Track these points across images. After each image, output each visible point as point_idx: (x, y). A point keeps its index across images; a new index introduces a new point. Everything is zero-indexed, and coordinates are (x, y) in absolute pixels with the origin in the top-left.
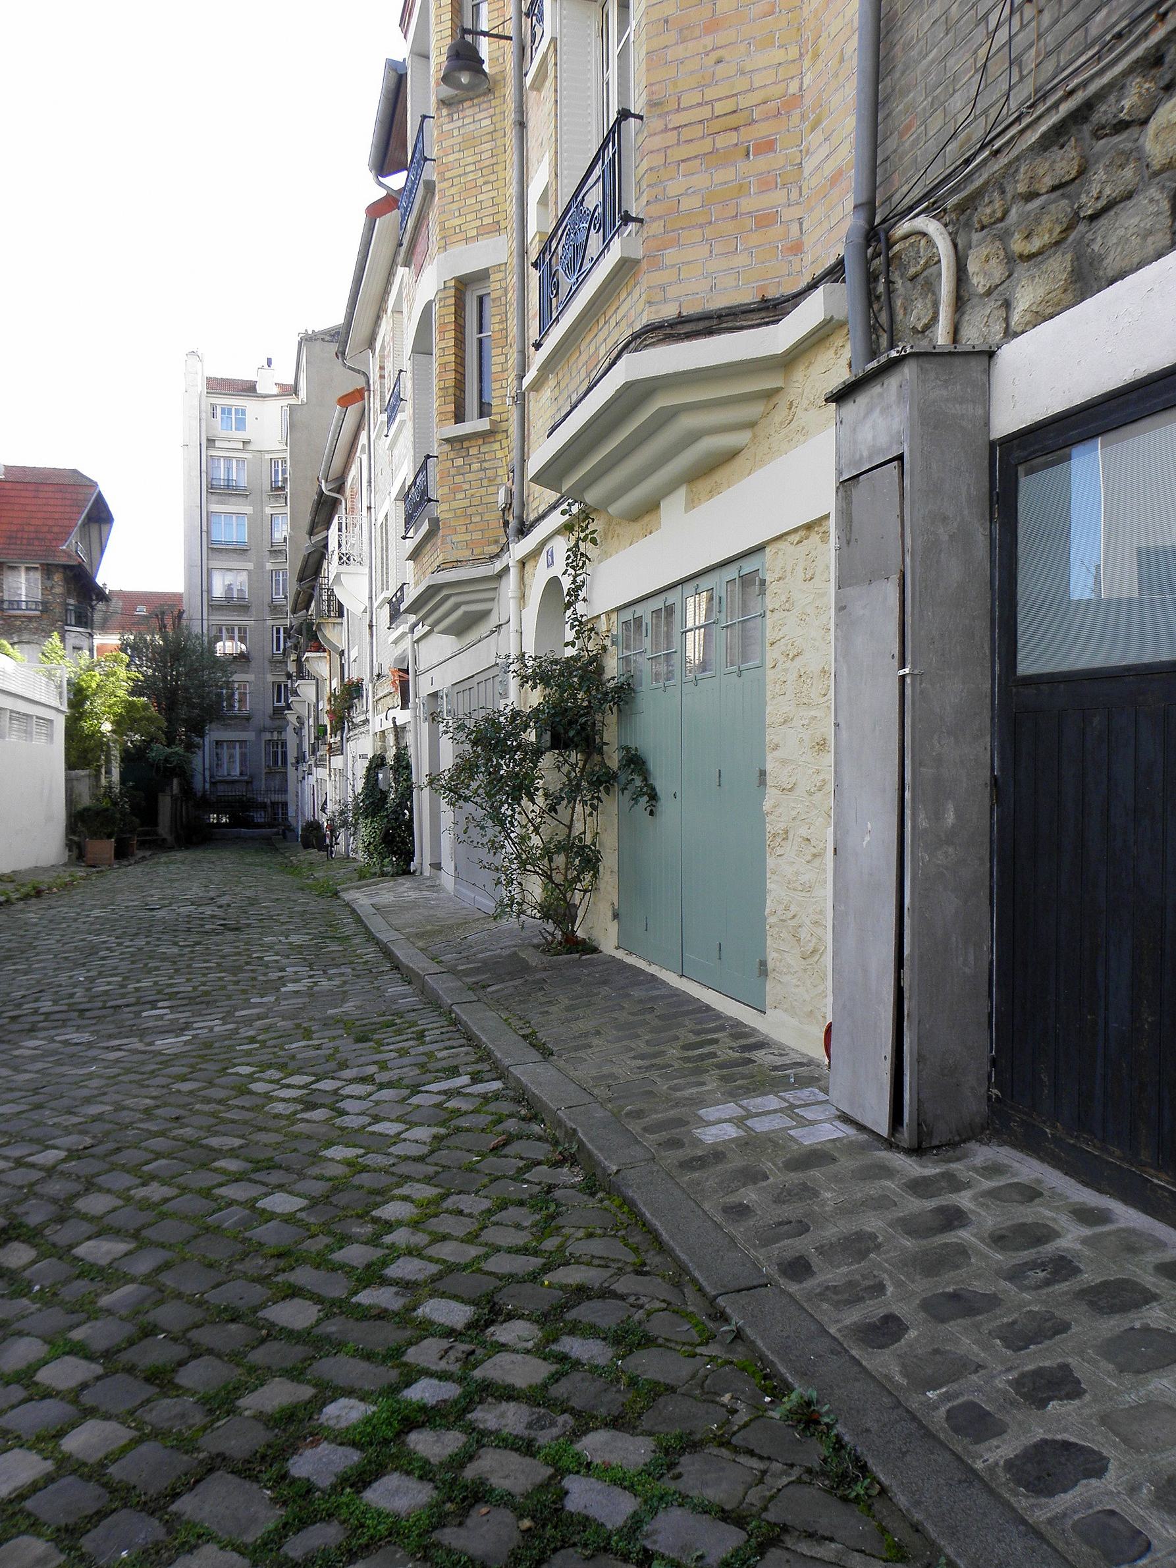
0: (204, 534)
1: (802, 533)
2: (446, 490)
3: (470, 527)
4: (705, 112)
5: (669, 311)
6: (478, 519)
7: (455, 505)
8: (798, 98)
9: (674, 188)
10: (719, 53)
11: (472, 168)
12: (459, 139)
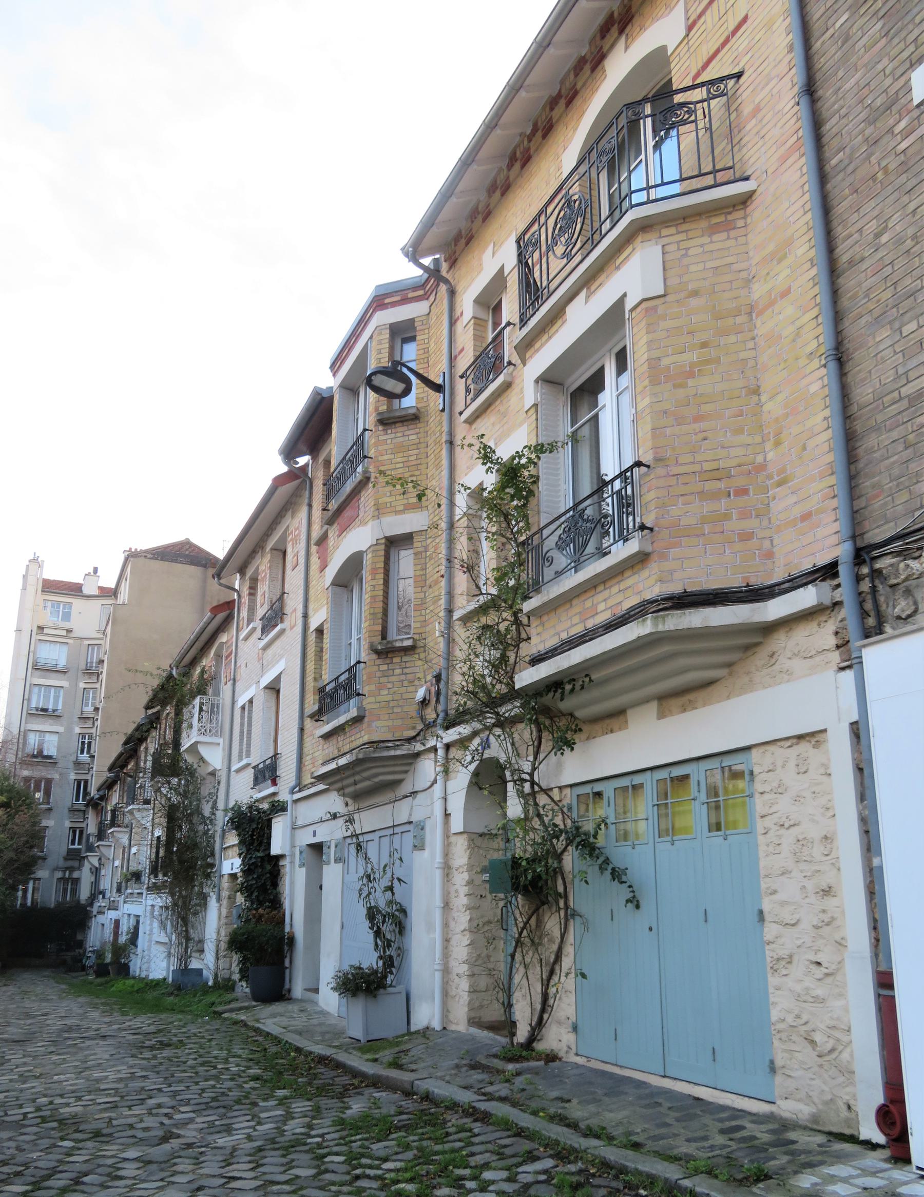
0: (26, 702)
1: (795, 741)
2: (373, 687)
3: (392, 716)
4: (697, 468)
5: (675, 588)
6: (399, 710)
7: (379, 698)
8: (762, 467)
9: (675, 511)
10: (704, 434)
11: (401, 465)
12: (392, 446)
